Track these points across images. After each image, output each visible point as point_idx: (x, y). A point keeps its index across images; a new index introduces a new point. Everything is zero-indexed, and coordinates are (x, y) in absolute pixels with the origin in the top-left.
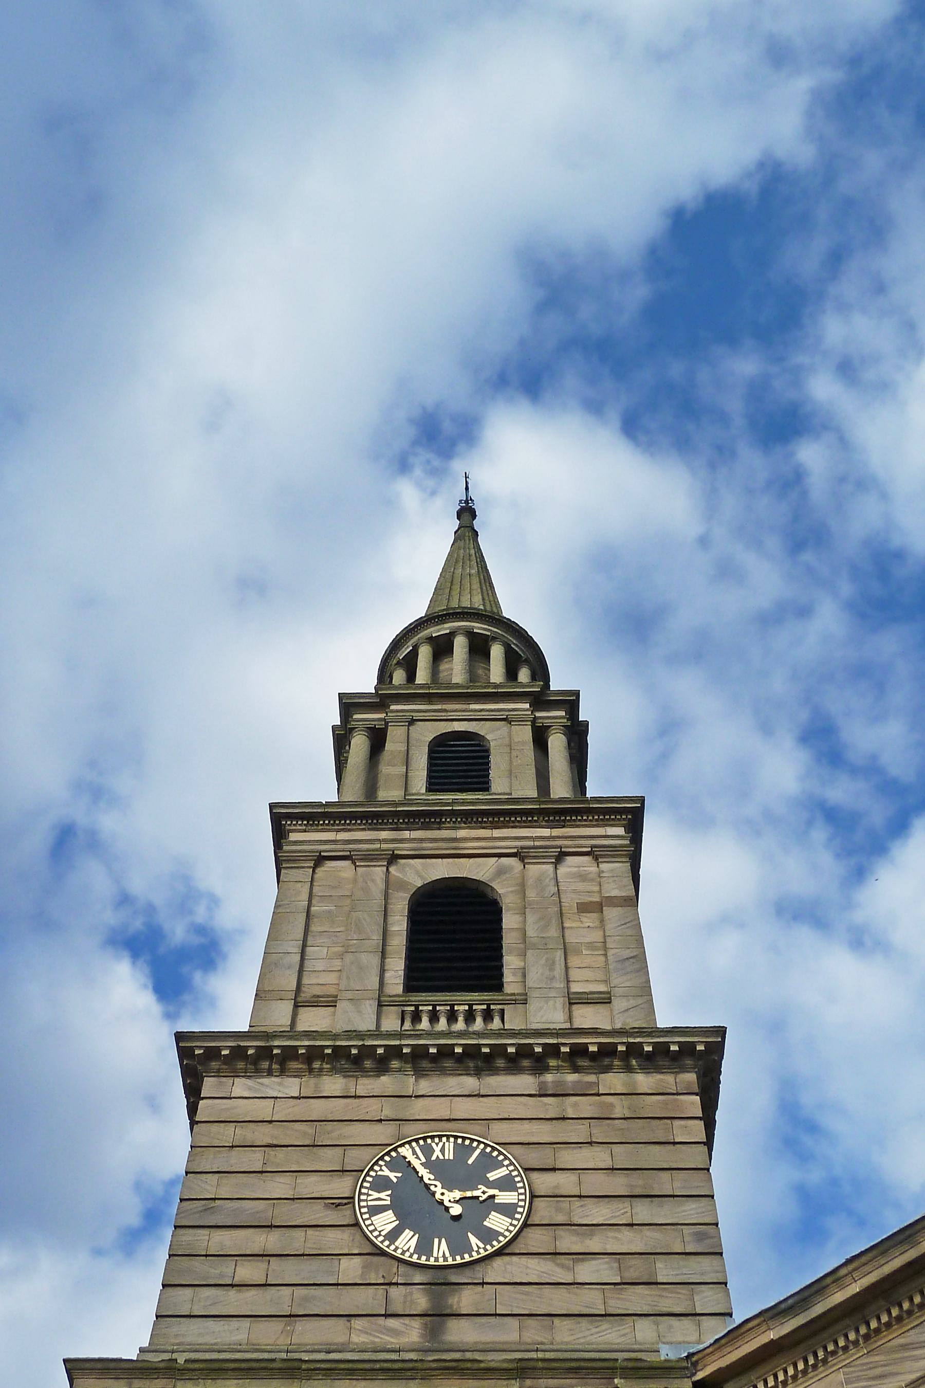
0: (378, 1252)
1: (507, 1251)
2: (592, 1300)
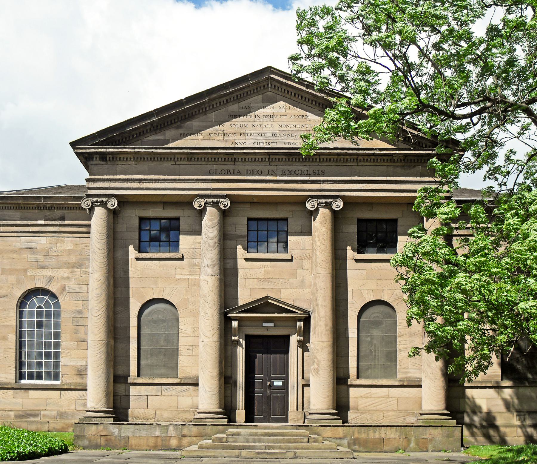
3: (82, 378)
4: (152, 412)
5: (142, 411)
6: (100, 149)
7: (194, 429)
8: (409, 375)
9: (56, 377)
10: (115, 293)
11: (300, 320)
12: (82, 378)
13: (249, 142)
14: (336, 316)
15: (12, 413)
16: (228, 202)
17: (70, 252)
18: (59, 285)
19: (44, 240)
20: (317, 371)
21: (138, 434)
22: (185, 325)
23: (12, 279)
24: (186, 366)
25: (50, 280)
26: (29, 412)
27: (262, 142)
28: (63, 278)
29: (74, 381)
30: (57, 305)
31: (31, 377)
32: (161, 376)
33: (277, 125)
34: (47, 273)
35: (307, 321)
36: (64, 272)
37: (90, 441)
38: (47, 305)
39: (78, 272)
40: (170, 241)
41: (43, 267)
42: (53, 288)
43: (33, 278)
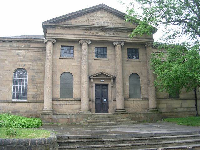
3: (35, 99)
4: (65, 110)
5: (61, 110)
6: (47, 26)
7: (81, 116)
8: (145, 97)
9: (25, 99)
10: (53, 70)
11: (112, 79)
12: (35, 99)
13: (96, 24)
14: (123, 77)
15: (10, 111)
16: (124, 44)
17: (31, 56)
18: (28, 67)
19: (23, 52)
20: (119, 96)
21: (62, 118)
22: (76, 81)
23: (12, 65)
24: (76, 94)
25: (25, 65)
26: (16, 111)
27: (100, 25)
28: (29, 65)
29: (32, 100)
30: (26, 74)
31: (17, 99)
32: (69, 98)
33: (101, 20)
34: (24, 63)
35: (114, 79)
36: (30, 63)
37: (46, 121)
38: (23, 74)
39: (34, 63)
40: (70, 54)
41: (22, 61)
42: (25, 68)
43: (19, 65)
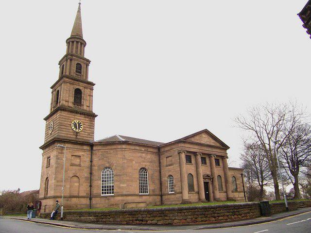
0: (193, 140)
1: (193, 140)
2: (86, 136)
33: (205, 140)
